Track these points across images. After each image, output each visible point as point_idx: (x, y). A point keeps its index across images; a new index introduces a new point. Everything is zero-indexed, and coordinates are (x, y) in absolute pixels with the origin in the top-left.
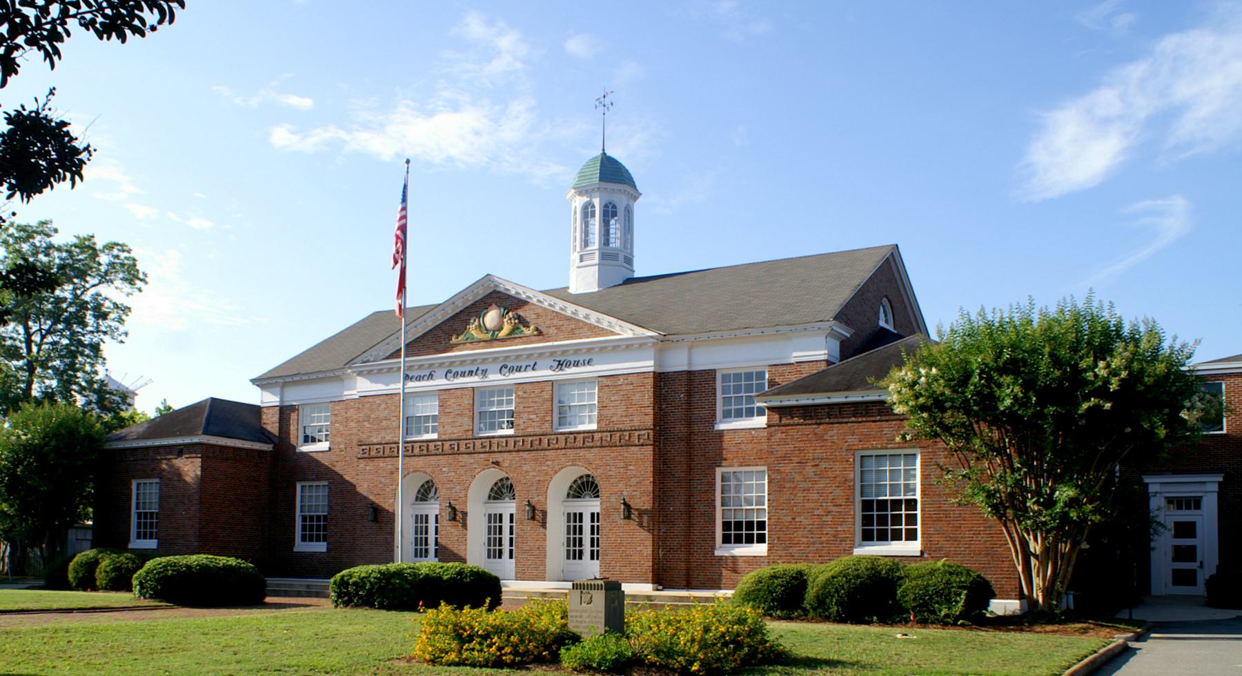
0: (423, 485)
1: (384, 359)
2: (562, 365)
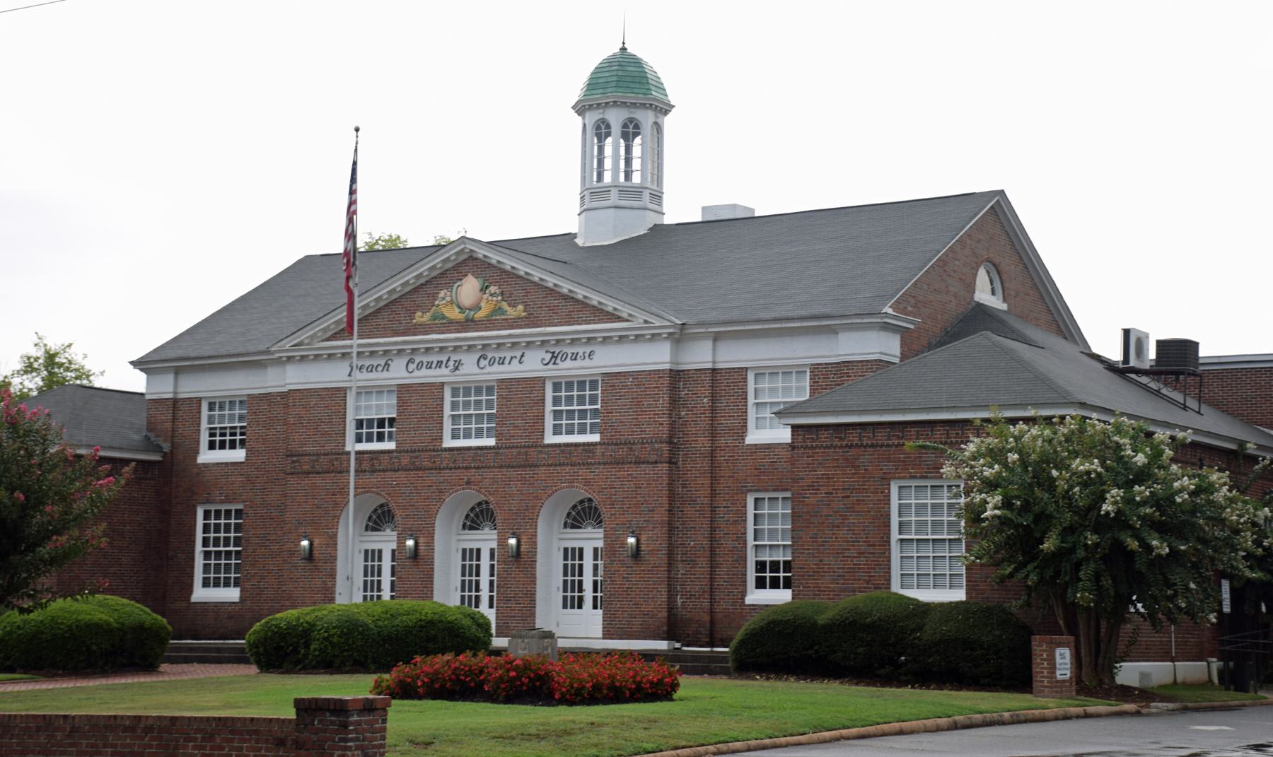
0: (376, 510)
1: (323, 341)
2: (556, 357)
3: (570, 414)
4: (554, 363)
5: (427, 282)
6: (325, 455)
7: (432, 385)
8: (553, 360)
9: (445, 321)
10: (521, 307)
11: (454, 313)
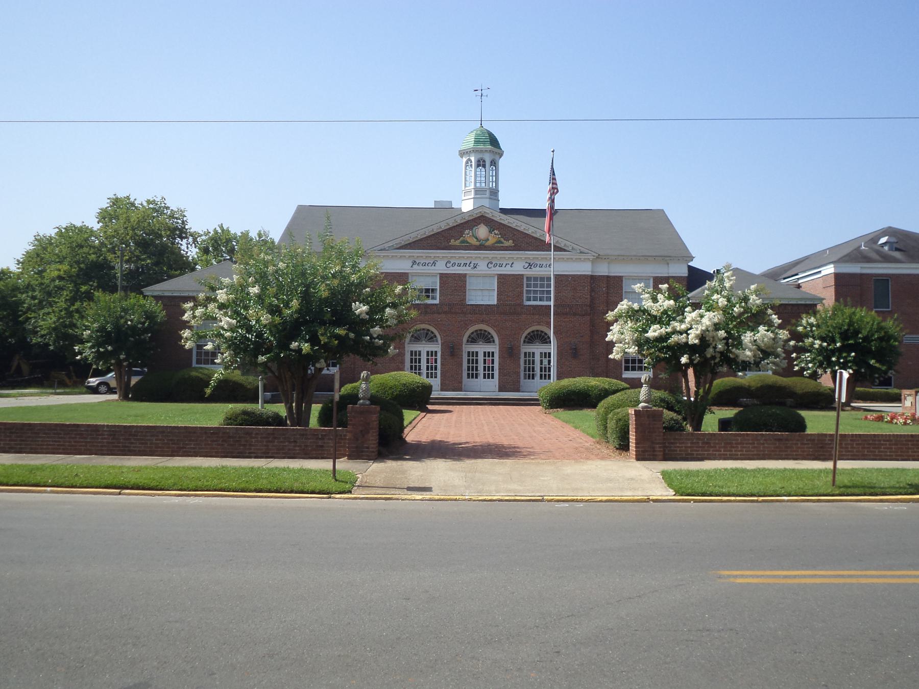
2: (531, 265)
3: (535, 292)
4: (530, 268)
9: (468, 244)
10: (511, 241)
11: (473, 241)
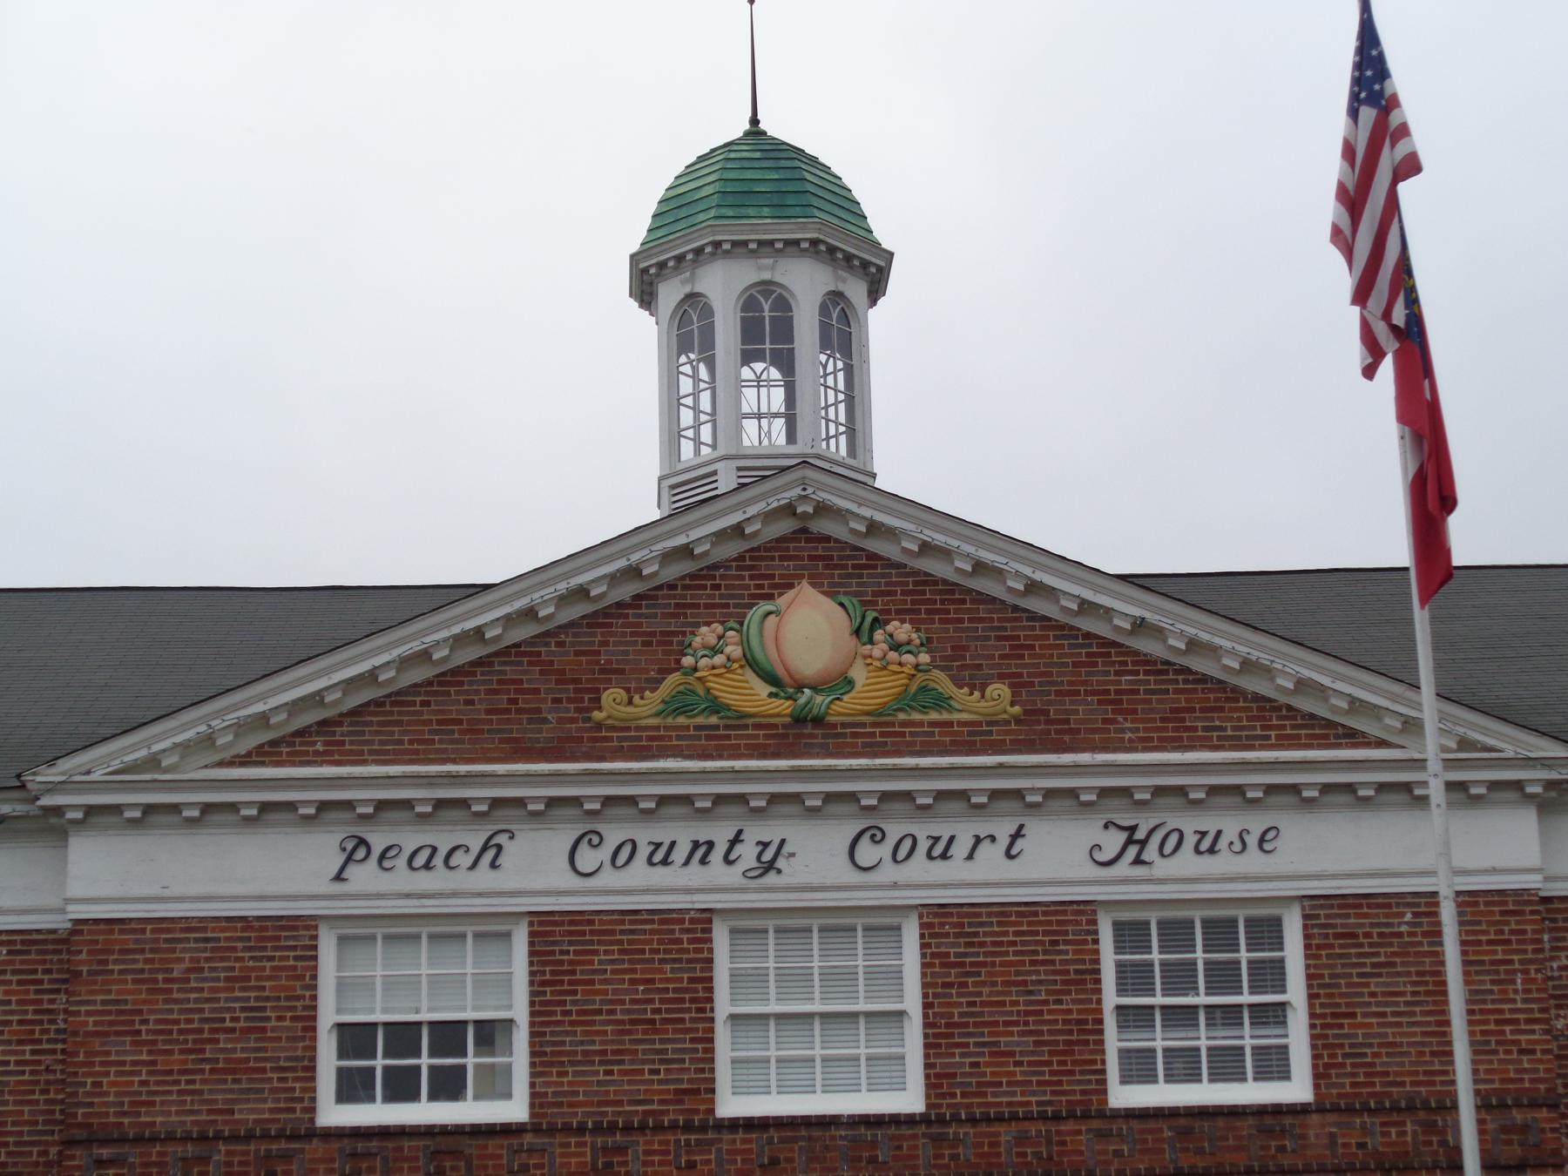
2: (1143, 843)
4: (1138, 861)
5: (638, 597)
6: (234, 1138)
7: (666, 918)
8: (1132, 851)
9: (714, 720)
11: (755, 696)
